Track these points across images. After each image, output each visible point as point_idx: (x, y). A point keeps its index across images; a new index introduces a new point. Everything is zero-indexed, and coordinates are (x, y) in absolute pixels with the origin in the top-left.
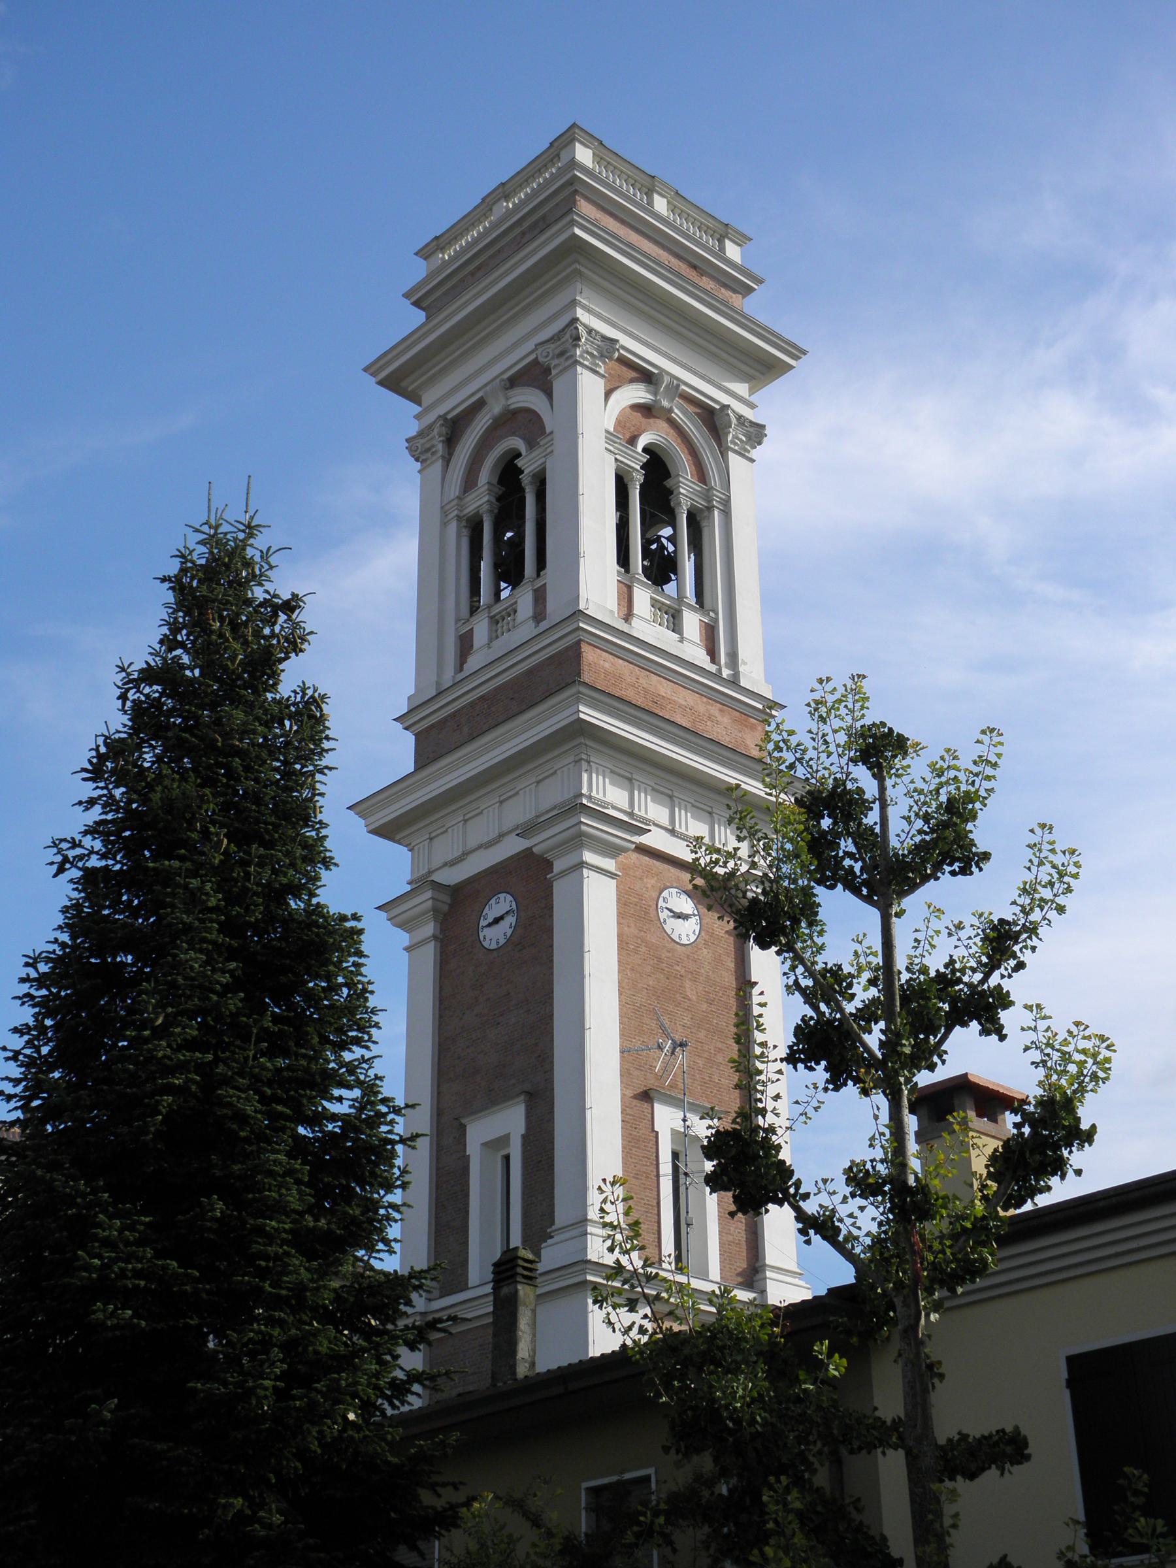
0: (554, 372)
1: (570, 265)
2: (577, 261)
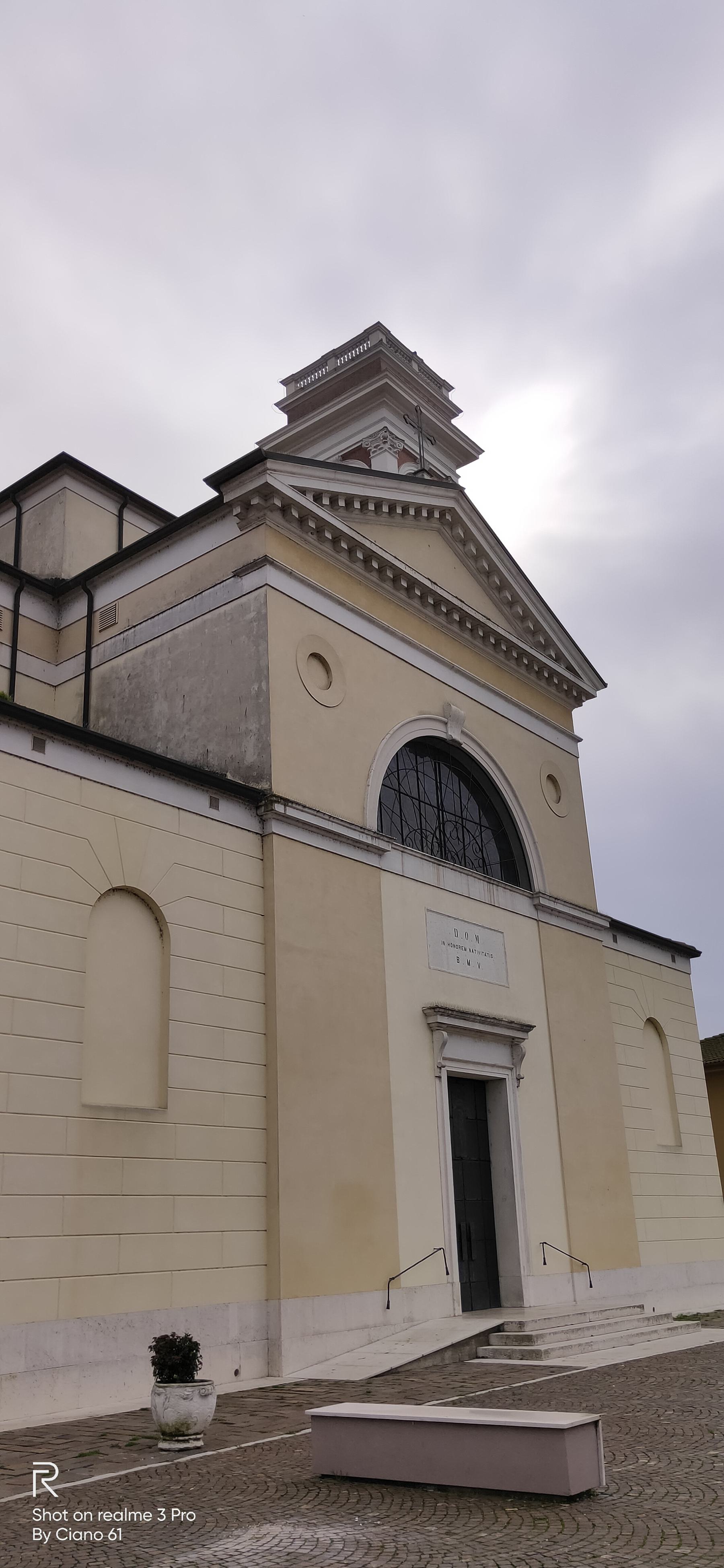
0: (372, 455)
1: (380, 379)
2: (386, 376)
